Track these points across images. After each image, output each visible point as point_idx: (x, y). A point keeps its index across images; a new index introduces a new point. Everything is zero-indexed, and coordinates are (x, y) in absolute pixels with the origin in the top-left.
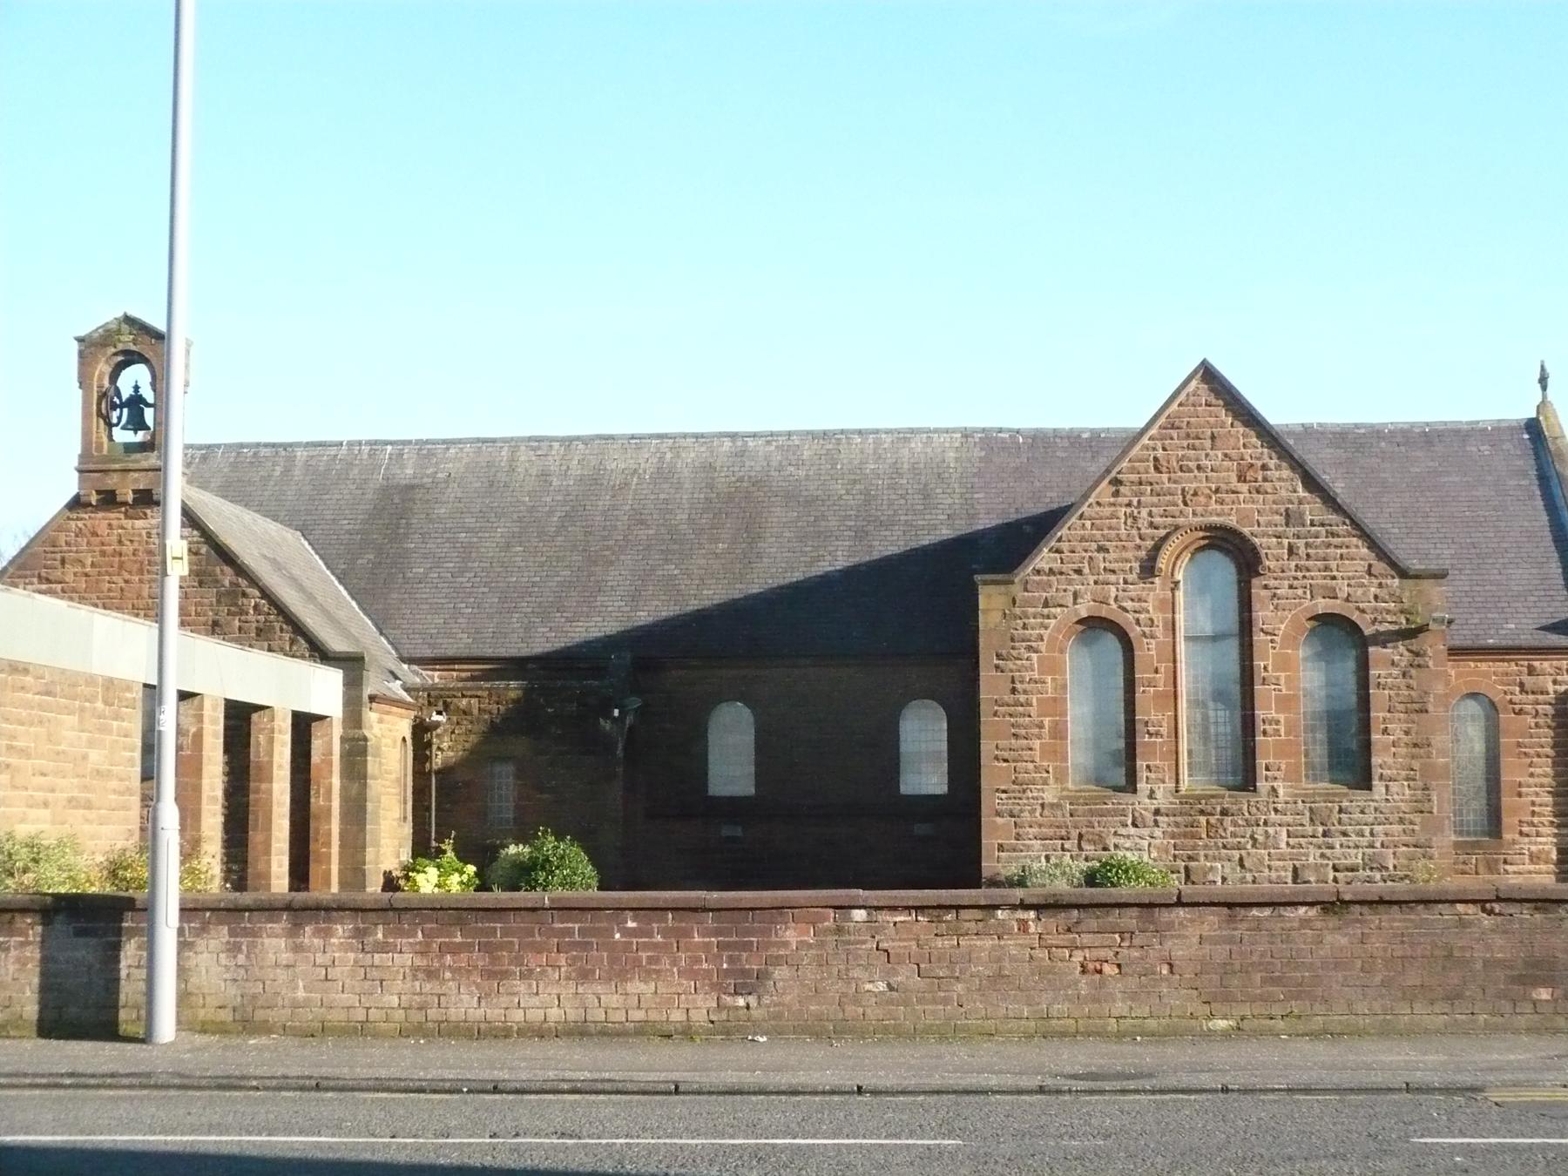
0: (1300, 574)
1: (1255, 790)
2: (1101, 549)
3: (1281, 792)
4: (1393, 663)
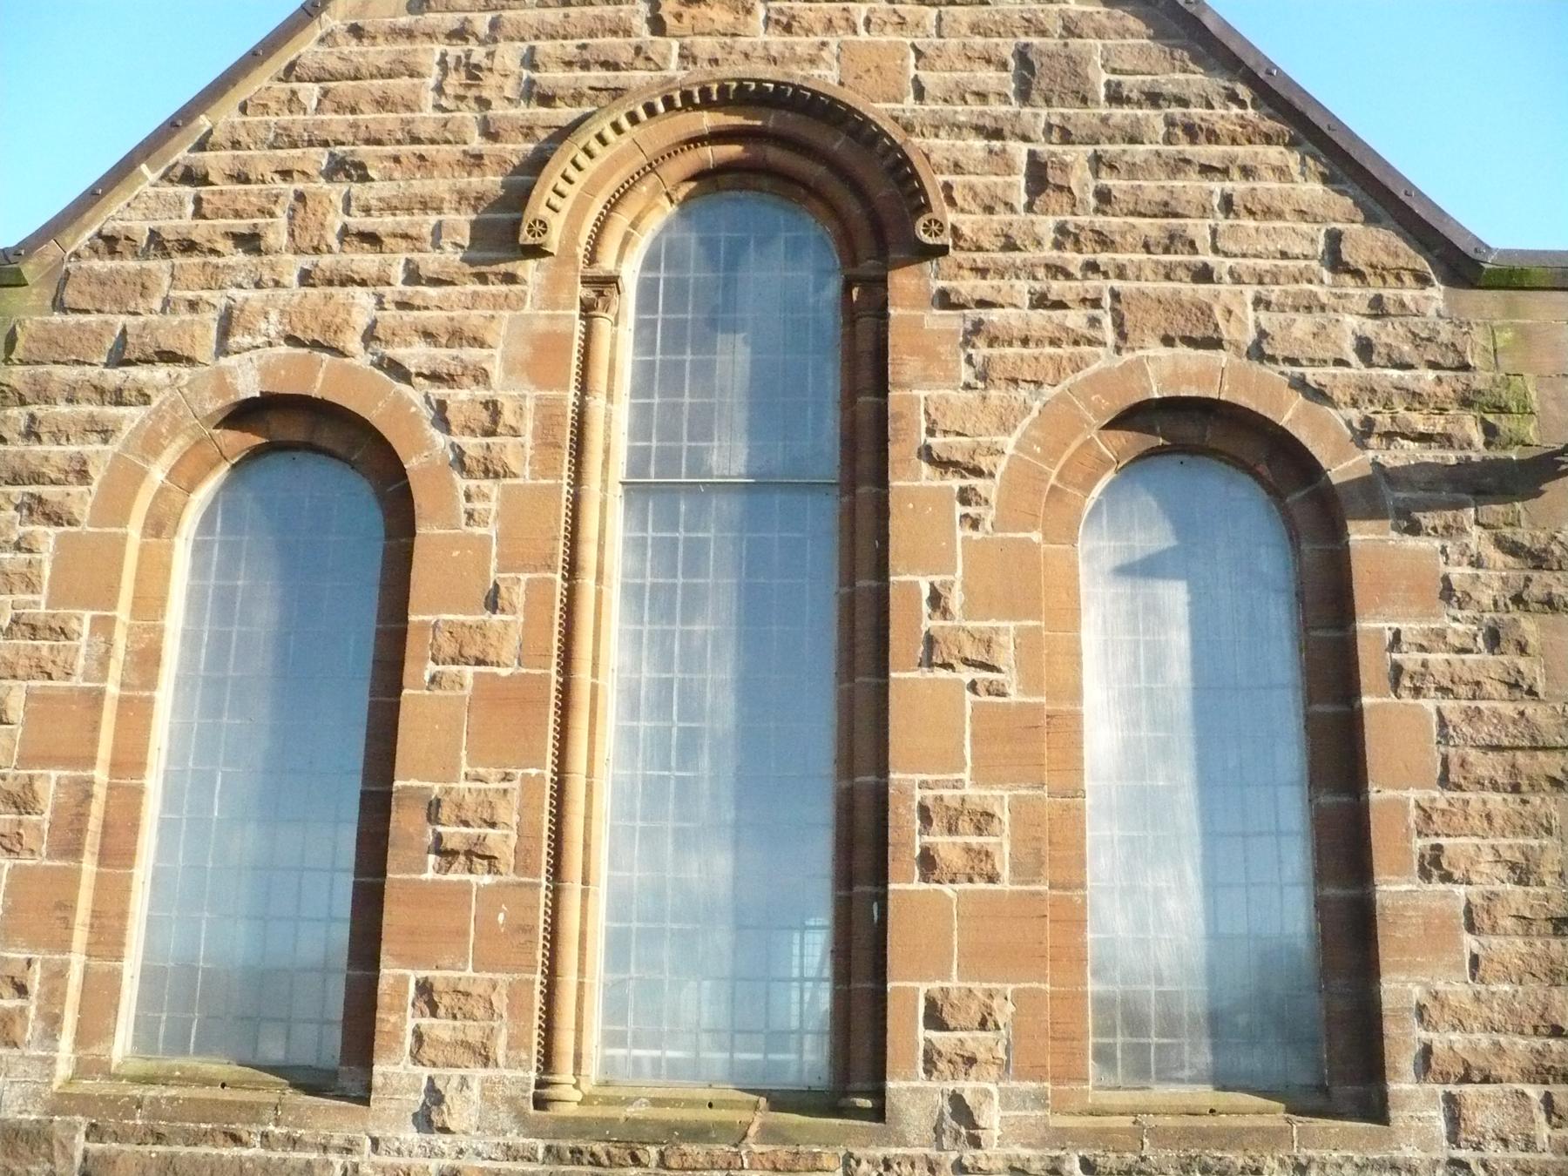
0: (1073, 260)
1: (878, 1114)
2: (340, 168)
3: (991, 1118)
4: (1447, 591)
